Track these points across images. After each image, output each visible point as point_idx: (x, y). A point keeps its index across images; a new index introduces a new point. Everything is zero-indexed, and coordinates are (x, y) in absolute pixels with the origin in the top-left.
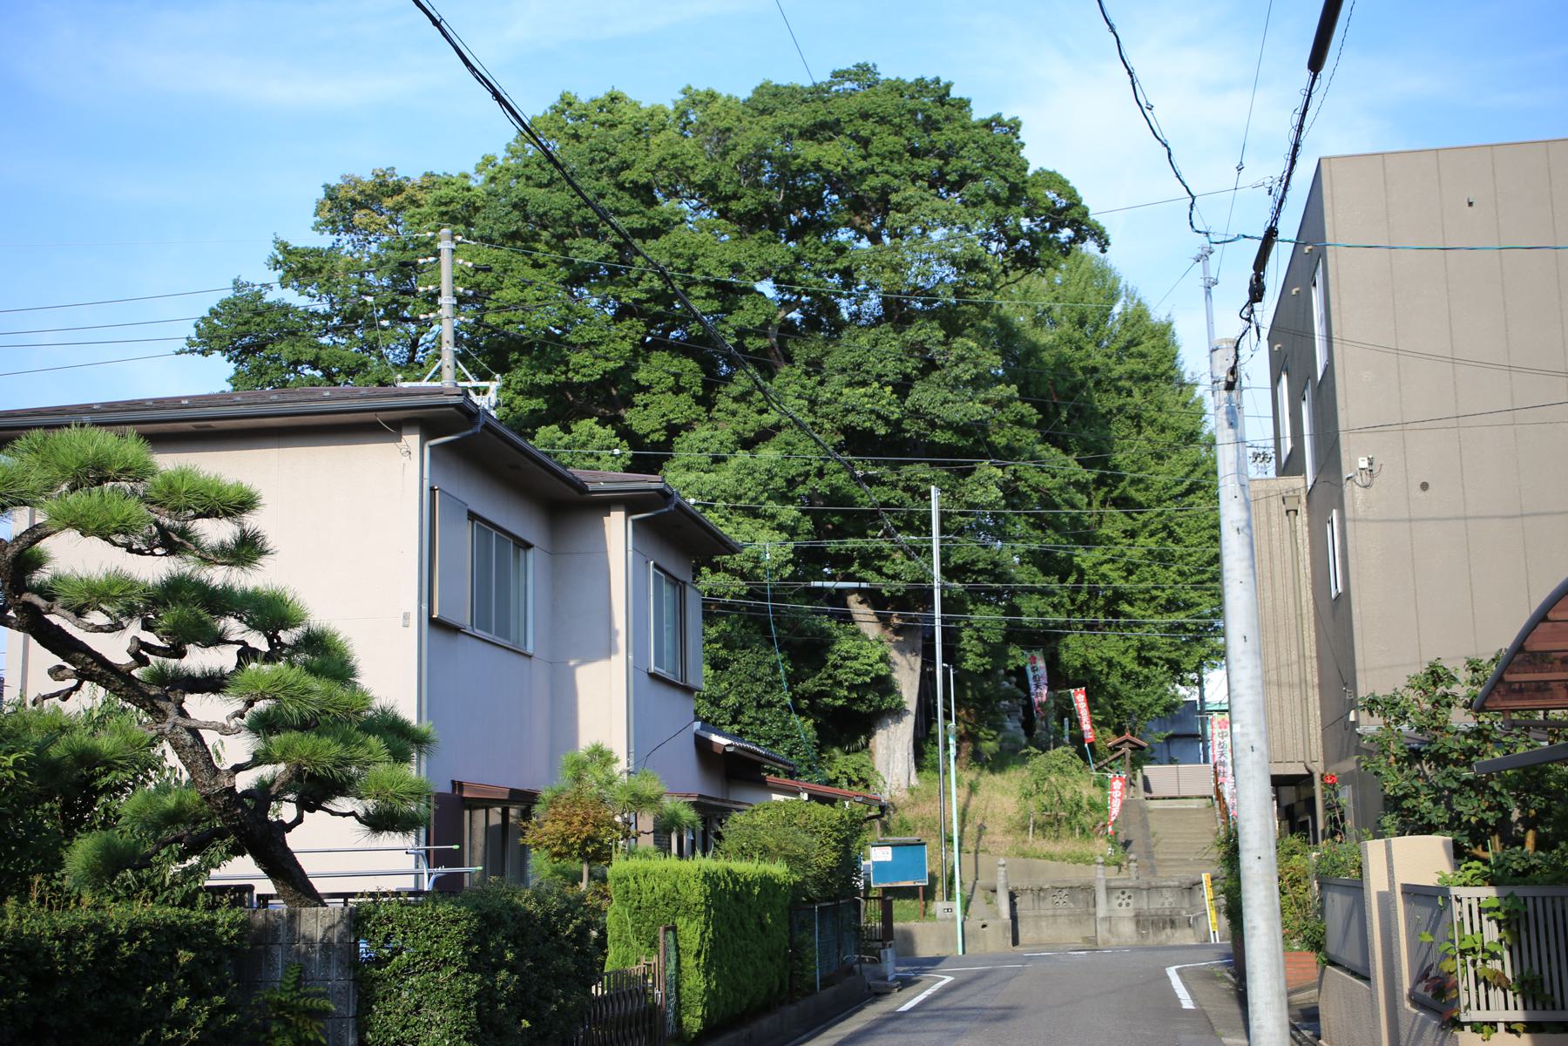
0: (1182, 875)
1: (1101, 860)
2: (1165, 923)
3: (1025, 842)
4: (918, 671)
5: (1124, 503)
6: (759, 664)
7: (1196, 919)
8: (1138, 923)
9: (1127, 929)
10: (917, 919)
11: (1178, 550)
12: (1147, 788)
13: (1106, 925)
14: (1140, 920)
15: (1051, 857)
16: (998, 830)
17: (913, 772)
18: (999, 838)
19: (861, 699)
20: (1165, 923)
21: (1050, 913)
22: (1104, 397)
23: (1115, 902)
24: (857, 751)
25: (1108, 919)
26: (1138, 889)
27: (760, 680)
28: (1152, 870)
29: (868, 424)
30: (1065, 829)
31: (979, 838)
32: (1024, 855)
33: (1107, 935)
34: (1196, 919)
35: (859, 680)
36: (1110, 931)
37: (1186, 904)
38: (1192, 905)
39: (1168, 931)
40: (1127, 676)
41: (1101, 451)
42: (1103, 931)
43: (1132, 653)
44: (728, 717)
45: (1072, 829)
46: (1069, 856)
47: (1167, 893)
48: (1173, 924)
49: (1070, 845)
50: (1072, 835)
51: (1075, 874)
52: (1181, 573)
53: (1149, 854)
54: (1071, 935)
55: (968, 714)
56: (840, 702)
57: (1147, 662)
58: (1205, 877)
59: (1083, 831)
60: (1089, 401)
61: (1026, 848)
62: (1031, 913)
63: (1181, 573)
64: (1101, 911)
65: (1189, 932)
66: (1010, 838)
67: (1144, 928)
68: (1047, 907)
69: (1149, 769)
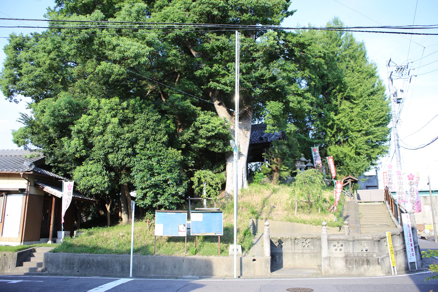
0: (376, 233)
1: (324, 223)
2: (363, 261)
3: (293, 214)
4: (249, 137)
5: (348, 98)
6: (148, 120)
7: (382, 259)
8: (346, 261)
9: (340, 265)
10: (216, 254)
11: (368, 112)
12: (359, 198)
13: (327, 262)
14: (348, 259)
15: (304, 222)
16: (280, 208)
17: (246, 182)
18: (280, 212)
19: (213, 145)
20: (363, 261)
21: (300, 251)
22: (340, 64)
23: (333, 248)
24: (219, 172)
25: (329, 258)
26: (347, 241)
27: (148, 128)
28: (358, 230)
29: (208, 9)
30: (314, 209)
31: (270, 212)
32: (291, 221)
33: (328, 268)
34: (382, 259)
35: (210, 134)
36: (329, 265)
37: (376, 251)
38: (380, 251)
39: (365, 266)
40: (351, 158)
41: (339, 78)
42: (325, 265)
43: (353, 151)
44: (126, 144)
45: (318, 209)
46: (314, 222)
47: (365, 244)
48: (368, 262)
49: (316, 216)
50: (317, 211)
51: (313, 231)
52: (370, 121)
53: (357, 221)
54: (312, 263)
55: (277, 161)
56: (201, 146)
57: (358, 154)
58: (388, 234)
59: (322, 210)
60: (336, 65)
61: (292, 217)
62: (290, 251)
63: (370, 121)
64: (325, 253)
65: (378, 267)
66: (286, 212)
67: (350, 264)
68: (299, 248)
69: (359, 191)
